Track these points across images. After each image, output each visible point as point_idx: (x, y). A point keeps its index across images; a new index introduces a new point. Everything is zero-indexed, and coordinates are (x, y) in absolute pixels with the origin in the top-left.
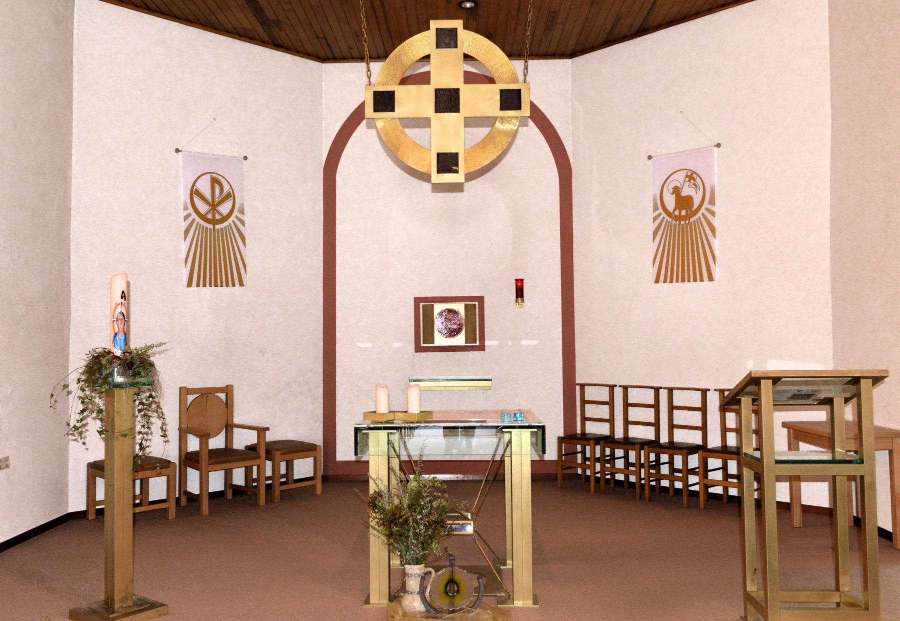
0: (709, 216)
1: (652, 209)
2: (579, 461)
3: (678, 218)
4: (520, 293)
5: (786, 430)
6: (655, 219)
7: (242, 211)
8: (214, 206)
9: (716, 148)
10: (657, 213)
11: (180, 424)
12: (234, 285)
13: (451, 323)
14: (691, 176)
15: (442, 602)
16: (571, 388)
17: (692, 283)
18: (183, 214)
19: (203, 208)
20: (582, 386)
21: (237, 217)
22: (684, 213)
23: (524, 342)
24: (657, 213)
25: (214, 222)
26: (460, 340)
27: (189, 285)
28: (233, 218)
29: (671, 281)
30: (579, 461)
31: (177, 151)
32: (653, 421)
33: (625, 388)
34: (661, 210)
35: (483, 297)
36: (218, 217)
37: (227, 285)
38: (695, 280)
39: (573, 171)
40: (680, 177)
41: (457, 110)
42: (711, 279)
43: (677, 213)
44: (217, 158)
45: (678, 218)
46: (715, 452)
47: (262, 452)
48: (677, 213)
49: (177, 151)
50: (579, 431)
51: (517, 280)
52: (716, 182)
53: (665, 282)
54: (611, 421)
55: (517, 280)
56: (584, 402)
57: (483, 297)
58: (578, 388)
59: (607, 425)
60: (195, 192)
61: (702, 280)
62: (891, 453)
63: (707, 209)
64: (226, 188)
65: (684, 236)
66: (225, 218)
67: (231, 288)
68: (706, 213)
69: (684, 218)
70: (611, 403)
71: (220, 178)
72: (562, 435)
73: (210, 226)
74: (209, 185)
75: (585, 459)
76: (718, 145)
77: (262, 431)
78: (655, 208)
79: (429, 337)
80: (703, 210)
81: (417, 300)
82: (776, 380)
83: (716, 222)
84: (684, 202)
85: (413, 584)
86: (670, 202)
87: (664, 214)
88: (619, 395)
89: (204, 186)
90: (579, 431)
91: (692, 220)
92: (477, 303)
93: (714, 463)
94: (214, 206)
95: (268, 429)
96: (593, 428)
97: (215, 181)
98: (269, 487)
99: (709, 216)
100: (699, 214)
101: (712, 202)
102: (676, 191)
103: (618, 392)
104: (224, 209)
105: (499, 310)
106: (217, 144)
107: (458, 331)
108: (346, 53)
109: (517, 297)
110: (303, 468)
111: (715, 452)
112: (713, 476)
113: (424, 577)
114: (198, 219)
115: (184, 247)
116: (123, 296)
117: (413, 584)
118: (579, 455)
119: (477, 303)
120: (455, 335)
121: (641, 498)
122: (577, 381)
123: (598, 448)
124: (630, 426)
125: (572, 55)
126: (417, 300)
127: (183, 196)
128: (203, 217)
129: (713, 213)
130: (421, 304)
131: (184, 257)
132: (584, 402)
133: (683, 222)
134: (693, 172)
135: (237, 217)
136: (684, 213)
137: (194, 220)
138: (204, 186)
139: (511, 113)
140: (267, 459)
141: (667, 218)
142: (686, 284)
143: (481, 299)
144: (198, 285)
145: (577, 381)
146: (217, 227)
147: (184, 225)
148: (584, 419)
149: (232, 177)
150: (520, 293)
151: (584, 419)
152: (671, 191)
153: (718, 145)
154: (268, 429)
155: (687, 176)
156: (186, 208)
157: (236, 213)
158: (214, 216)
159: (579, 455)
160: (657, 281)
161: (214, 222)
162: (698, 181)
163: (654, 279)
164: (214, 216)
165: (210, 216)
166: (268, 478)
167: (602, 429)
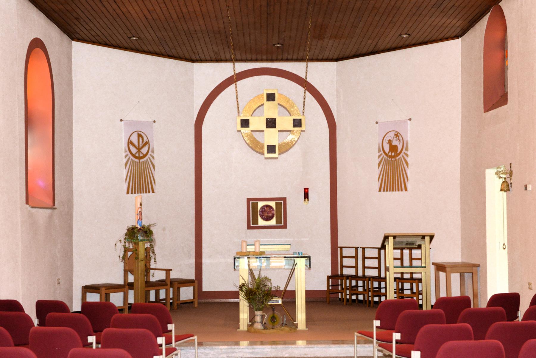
0: (405, 157)
1: (377, 151)
2: (340, 289)
3: (391, 157)
4: (306, 196)
5: (434, 266)
6: (379, 156)
7: (153, 152)
8: (139, 149)
9: (409, 122)
10: (380, 153)
11: (124, 267)
12: (149, 192)
13: (265, 213)
14: (397, 135)
15: (270, 325)
16: (336, 250)
17: (397, 192)
18: (124, 155)
19: (134, 150)
20: (341, 248)
21: (151, 155)
22: (393, 154)
23: (309, 222)
24: (380, 153)
25: (139, 158)
26: (273, 222)
27: (128, 193)
28: (148, 155)
29: (387, 191)
30: (340, 289)
31: (121, 120)
32: (377, 266)
33: (364, 249)
34: (382, 152)
35: (286, 198)
36: (141, 155)
37: (146, 193)
38: (399, 191)
39: (337, 128)
40: (392, 135)
41: (275, 127)
42: (406, 190)
43: (390, 154)
44: (139, 123)
45: (391, 157)
46: (407, 280)
47: (169, 283)
48: (390, 154)
49: (121, 120)
50: (339, 273)
51: (305, 189)
52: (409, 139)
53: (384, 191)
54: (356, 267)
55: (305, 189)
56: (342, 257)
57: (286, 198)
58: (339, 249)
59: (354, 269)
60: (130, 143)
61: (402, 191)
62: (473, 273)
63: (404, 153)
64: (145, 139)
65: (393, 168)
66: (145, 156)
67: (148, 194)
68: (404, 155)
69: (393, 157)
70: (356, 257)
71: (141, 133)
72: (330, 274)
73: (137, 160)
74: (137, 138)
75: (342, 288)
76: (410, 119)
77: (168, 271)
78: (379, 151)
79: (256, 221)
80: (402, 153)
81: (249, 200)
82: (395, 237)
83: (409, 160)
84: (393, 148)
85: (258, 319)
86: (387, 148)
87: (383, 154)
88: (360, 252)
89: (134, 139)
90: (339, 273)
91: (397, 158)
92: (282, 202)
93: (407, 285)
94: (139, 149)
95: (171, 270)
96: (347, 272)
97: (139, 136)
98: (171, 303)
99: (405, 157)
100: (401, 155)
101: (407, 149)
102: (390, 142)
103: (360, 251)
104: (144, 150)
105: (295, 207)
106: (139, 116)
107: (271, 218)
108: (208, 58)
109: (305, 198)
110: (187, 294)
111: (407, 280)
112: (406, 292)
113: (262, 317)
114: (132, 157)
115: (125, 172)
116: (141, 205)
117: (258, 319)
118: (340, 286)
119: (282, 202)
120: (270, 220)
121: (369, 306)
122: (339, 246)
123: (348, 281)
124: (366, 269)
125: (337, 60)
126: (249, 200)
127: (124, 144)
128: (134, 156)
129: (407, 155)
130: (251, 202)
131: (125, 179)
132: (342, 257)
133: (393, 159)
134: (398, 133)
135: (151, 155)
136: (393, 154)
137: (129, 158)
138: (134, 139)
139: (296, 129)
140: (171, 287)
141: (385, 156)
142: (394, 192)
143: (284, 199)
144: (132, 193)
145: (339, 246)
146: (141, 160)
147: (125, 161)
148: (342, 266)
149: (144, 130)
150: (306, 196)
151: (342, 266)
152: (387, 142)
153: (410, 119)
154: (171, 270)
155: (395, 135)
156: (126, 151)
157: (150, 153)
158: (139, 155)
159: (340, 286)
160: (380, 191)
161: (139, 158)
162: (400, 137)
163: (378, 189)
164: (139, 155)
165: (137, 155)
166: (171, 299)
167: (351, 272)
